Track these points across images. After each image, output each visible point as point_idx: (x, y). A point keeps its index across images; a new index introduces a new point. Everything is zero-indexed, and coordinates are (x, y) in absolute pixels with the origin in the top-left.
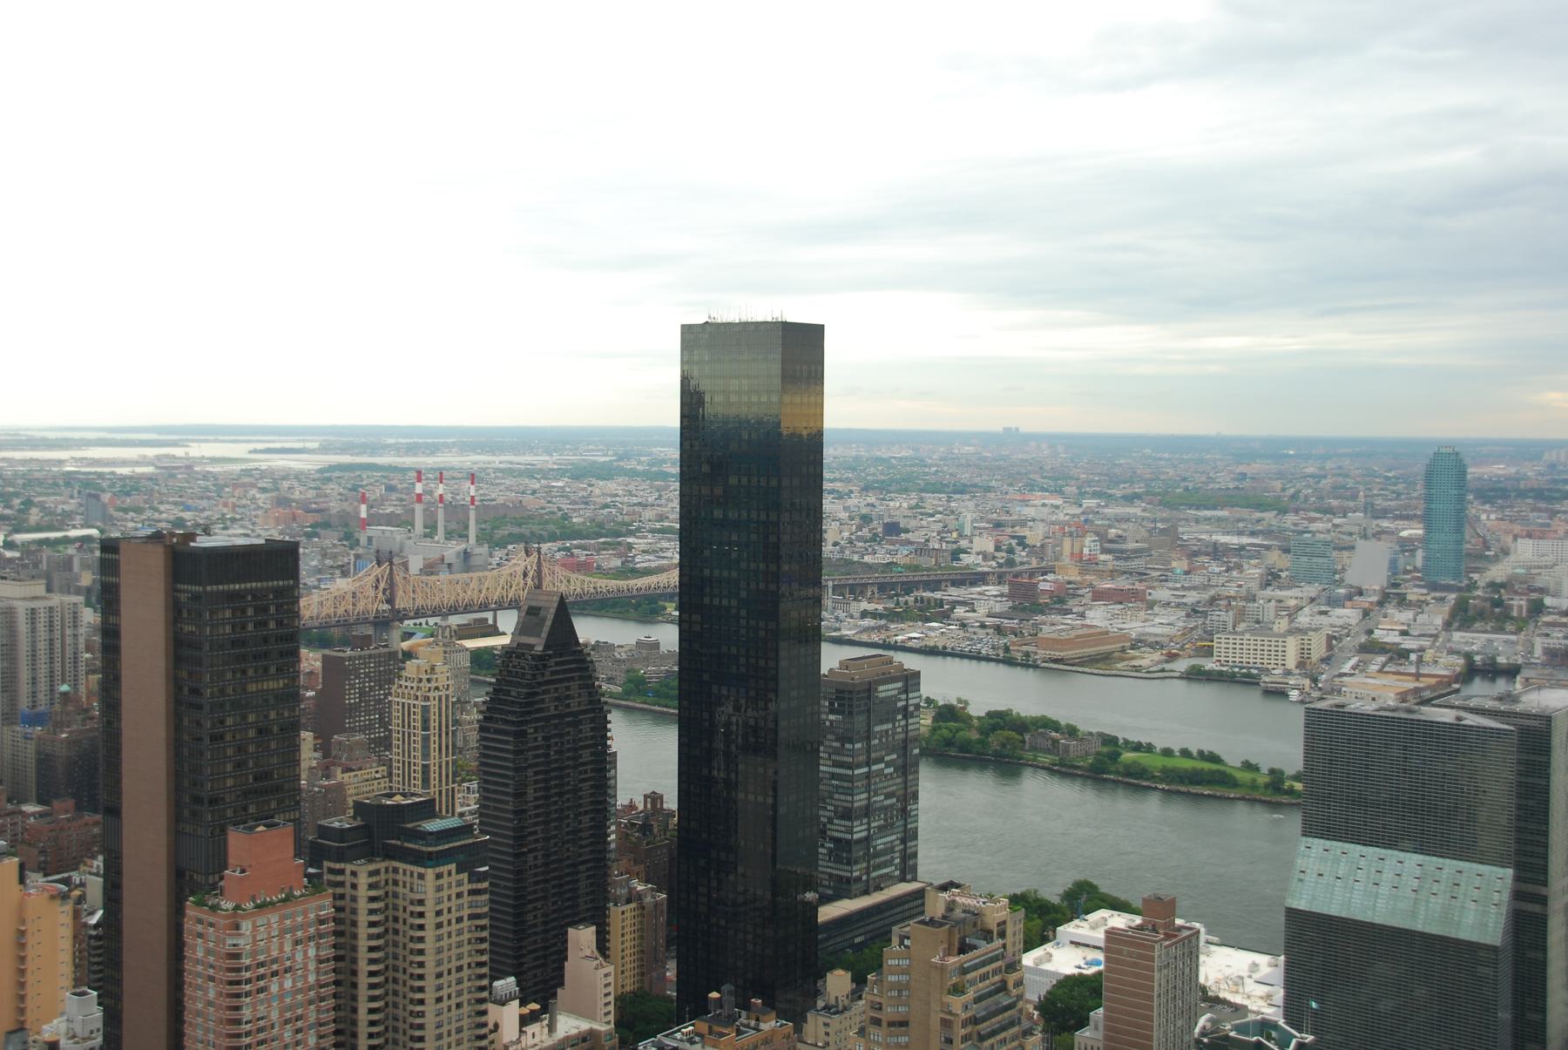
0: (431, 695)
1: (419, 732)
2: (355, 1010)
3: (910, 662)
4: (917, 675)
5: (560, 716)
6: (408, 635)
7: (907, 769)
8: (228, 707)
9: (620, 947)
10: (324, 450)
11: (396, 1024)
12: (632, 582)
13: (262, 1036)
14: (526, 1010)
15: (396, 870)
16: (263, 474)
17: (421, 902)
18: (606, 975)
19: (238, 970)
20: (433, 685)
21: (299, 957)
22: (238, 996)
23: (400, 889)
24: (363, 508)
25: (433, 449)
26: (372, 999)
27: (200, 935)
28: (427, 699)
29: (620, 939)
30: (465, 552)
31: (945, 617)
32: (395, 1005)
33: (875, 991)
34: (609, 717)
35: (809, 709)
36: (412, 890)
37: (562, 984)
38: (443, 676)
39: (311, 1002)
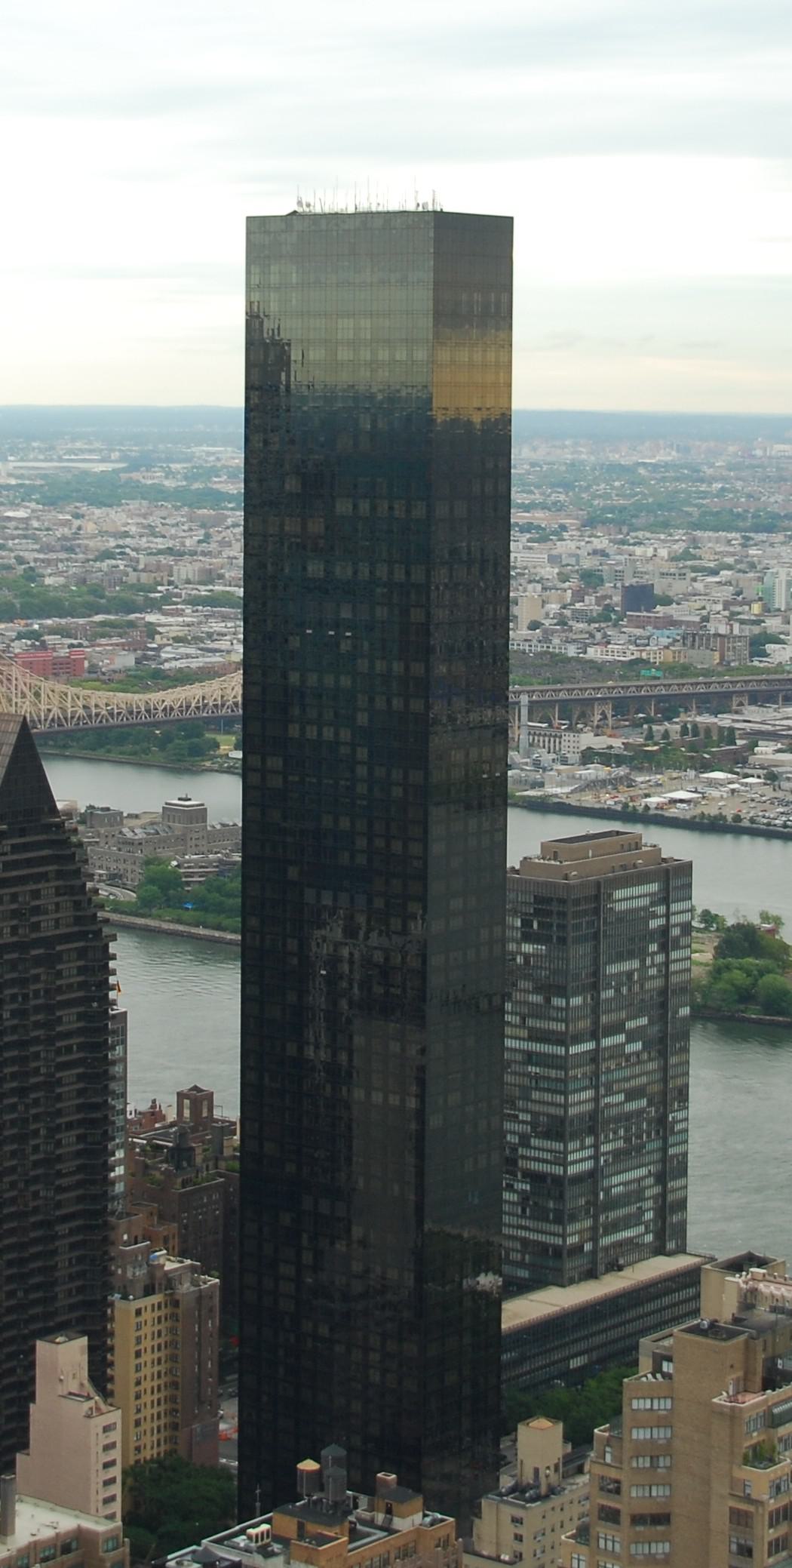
3: (674, 845)
5: (22, 947)
9: (133, 1376)
12: (155, 697)
18: (106, 1429)
31: (737, 761)
33: (608, 1458)
34: (113, 948)
37: (24, 1446)
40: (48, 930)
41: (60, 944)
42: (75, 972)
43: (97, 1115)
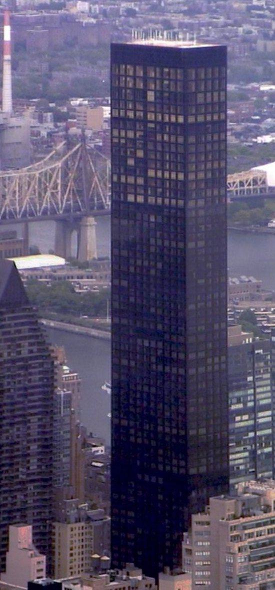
5: (13, 361)
9: (69, 565)
18: (39, 563)
29: (69, 558)
33: (188, 543)
35: (216, 326)
40: (25, 353)
41: (30, 360)
42: (36, 427)
43: (49, 403)
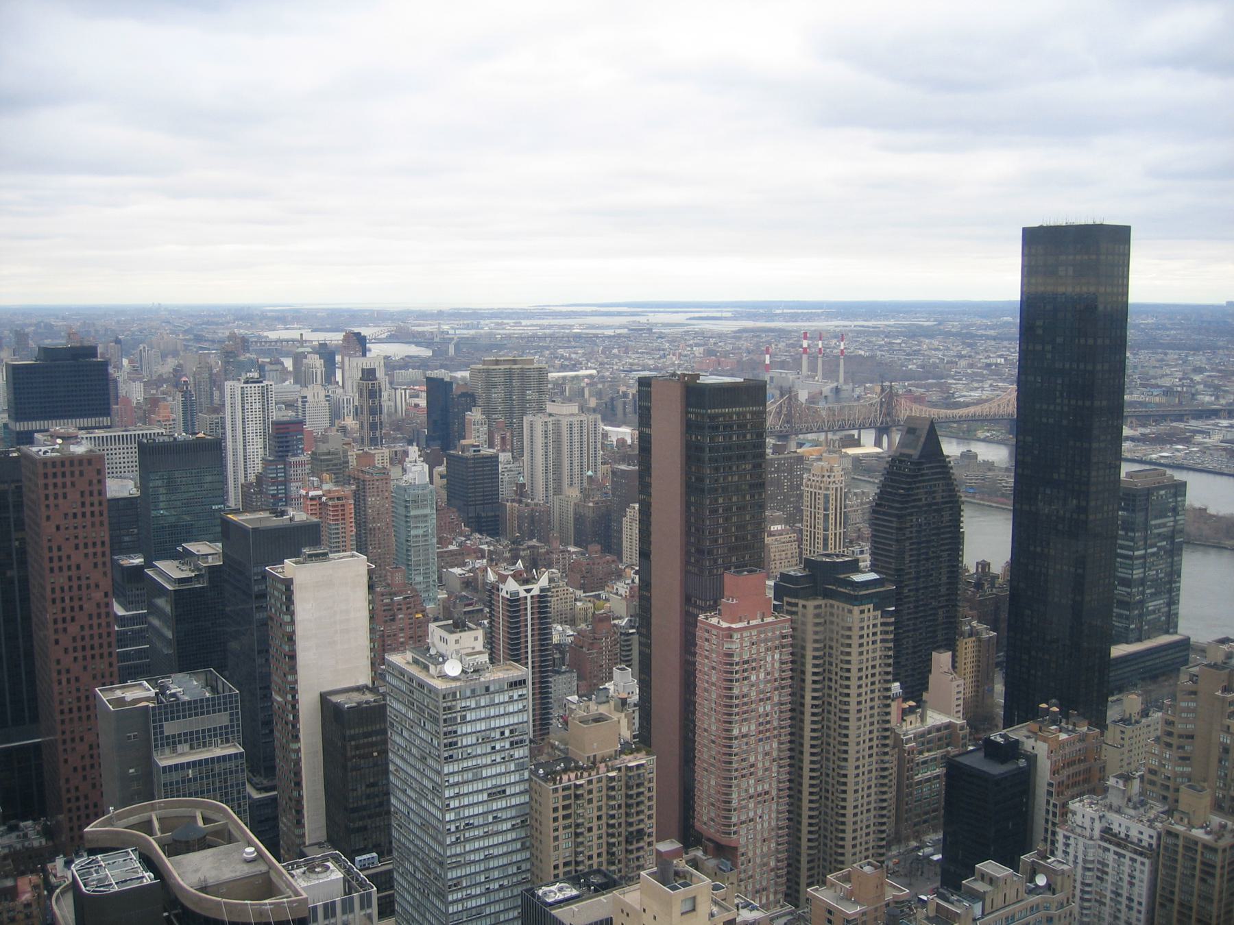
0: (831, 486)
1: (822, 511)
2: (803, 697)
3: (1179, 476)
4: (1184, 484)
6: (800, 445)
7: (1174, 552)
8: (720, 490)
10: (735, 318)
11: (829, 708)
12: (956, 412)
13: (745, 708)
14: (906, 705)
15: (832, 606)
16: (701, 334)
17: (850, 629)
18: (958, 686)
19: (732, 664)
20: (832, 479)
21: (769, 659)
22: (731, 681)
23: (835, 619)
24: (767, 357)
25: (810, 317)
26: (814, 690)
27: (707, 640)
28: (827, 489)
30: (837, 388)
31: (1187, 441)
32: (830, 696)
34: (962, 507)
36: (843, 620)
37: (926, 689)
38: (838, 473)
39: (776, 689)
40: (939, 500)
